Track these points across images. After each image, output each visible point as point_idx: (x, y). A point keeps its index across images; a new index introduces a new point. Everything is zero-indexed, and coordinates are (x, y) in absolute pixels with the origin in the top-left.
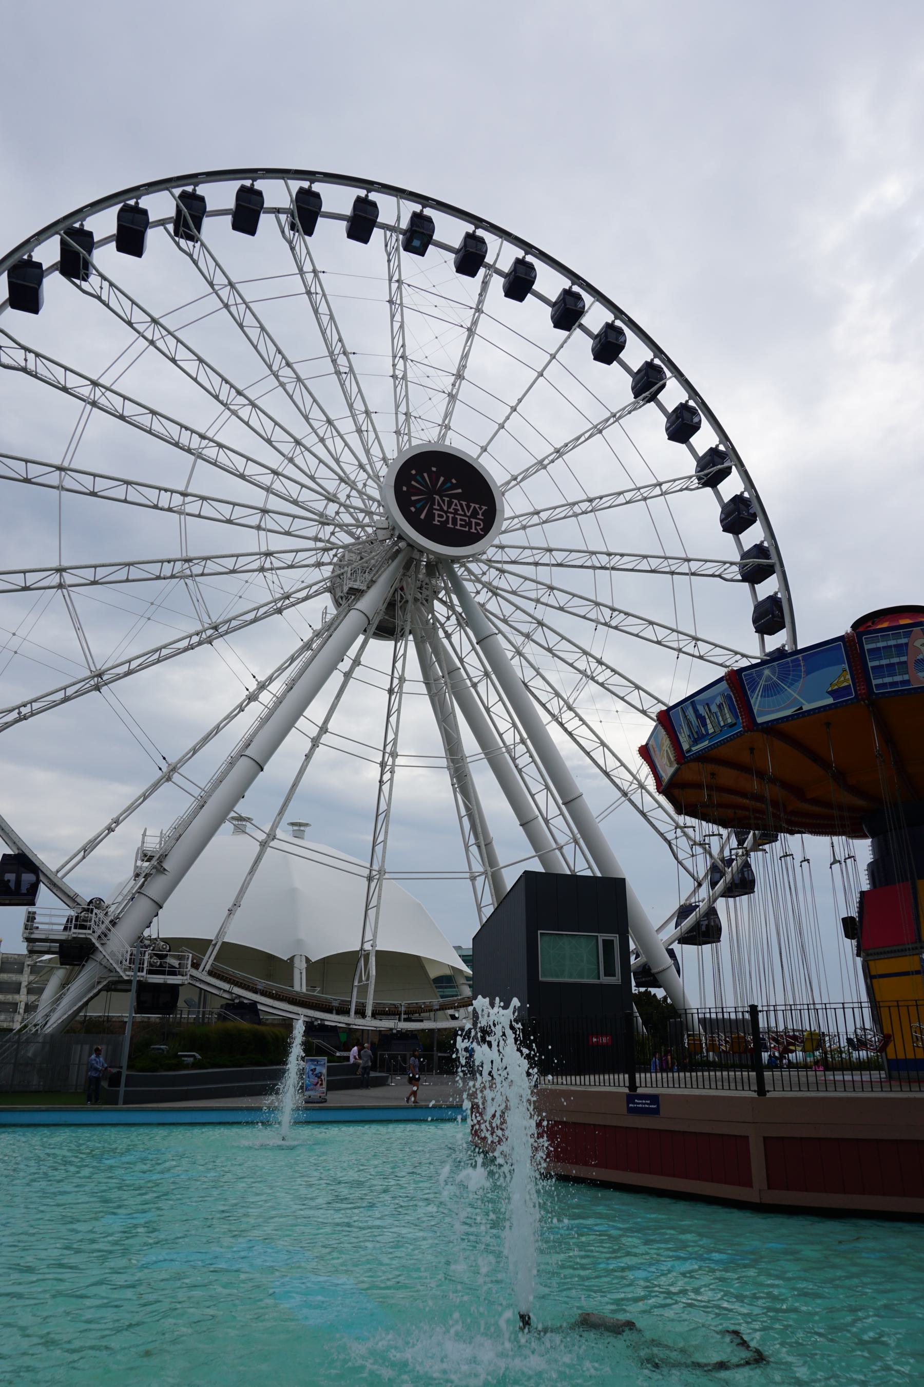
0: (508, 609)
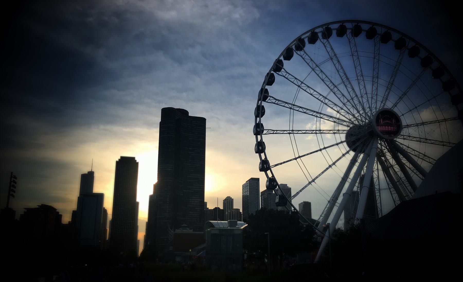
0: (351, 110)
